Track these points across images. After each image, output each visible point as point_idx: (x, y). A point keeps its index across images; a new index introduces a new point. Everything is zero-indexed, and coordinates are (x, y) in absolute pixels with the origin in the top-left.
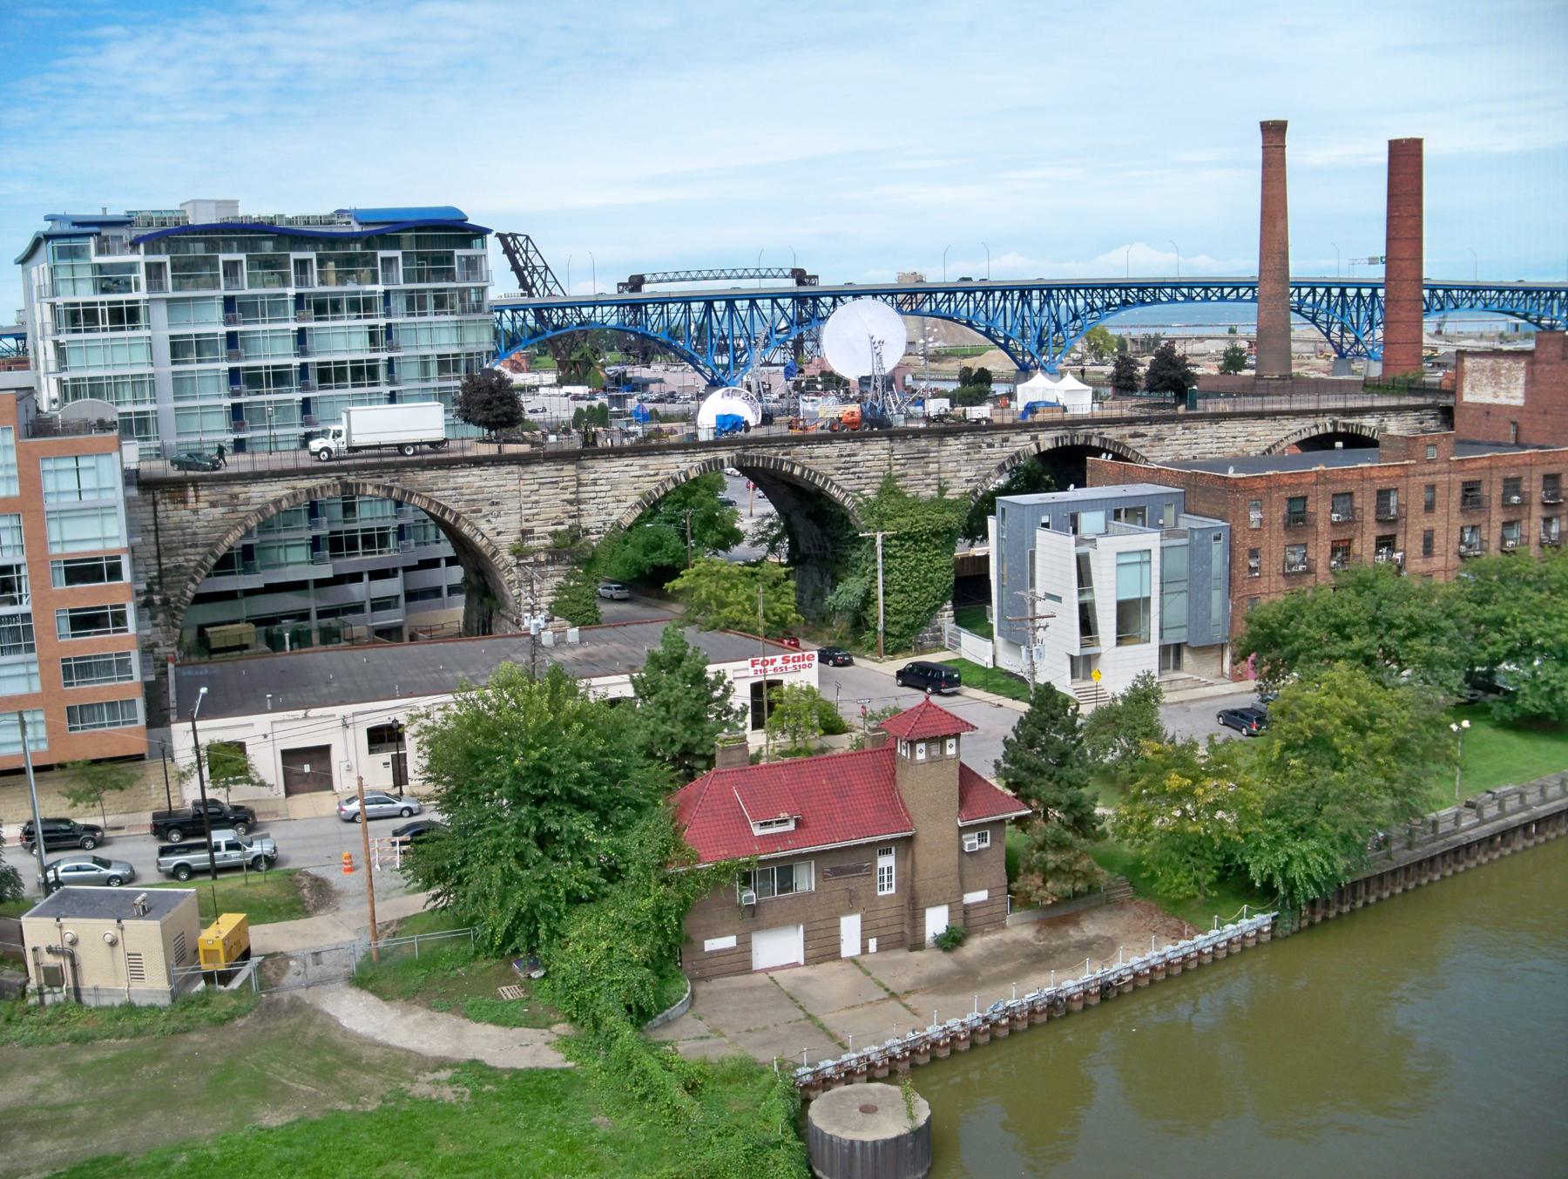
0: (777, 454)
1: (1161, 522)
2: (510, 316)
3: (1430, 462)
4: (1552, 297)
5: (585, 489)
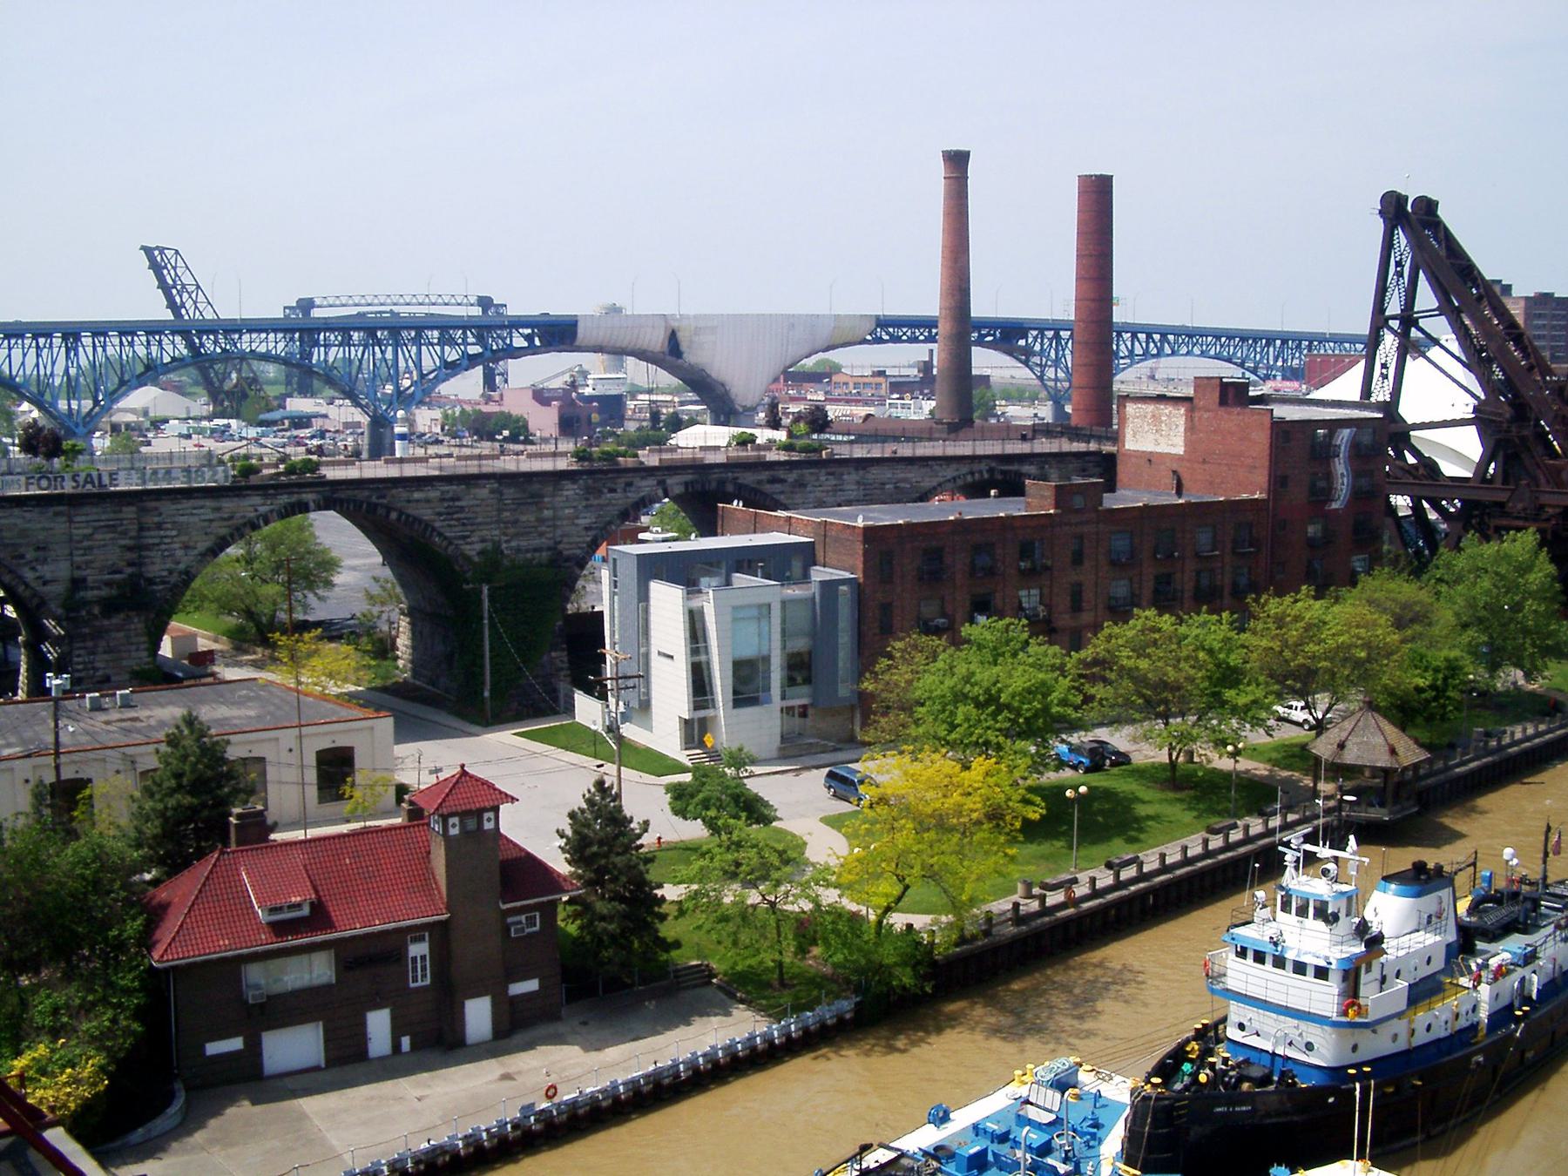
0: (371, 497)
1: (788, 574)
2: (144, 339)
3: (1078, 511)
4: (1268, 345)
5: (147, 534)
